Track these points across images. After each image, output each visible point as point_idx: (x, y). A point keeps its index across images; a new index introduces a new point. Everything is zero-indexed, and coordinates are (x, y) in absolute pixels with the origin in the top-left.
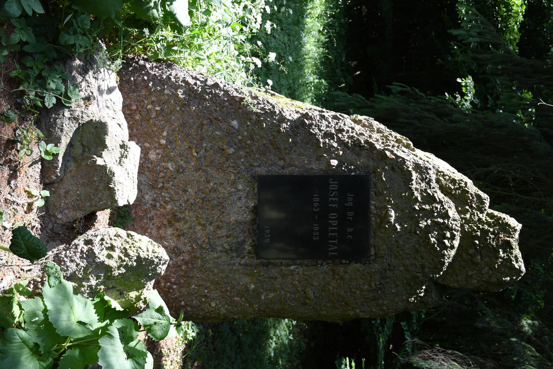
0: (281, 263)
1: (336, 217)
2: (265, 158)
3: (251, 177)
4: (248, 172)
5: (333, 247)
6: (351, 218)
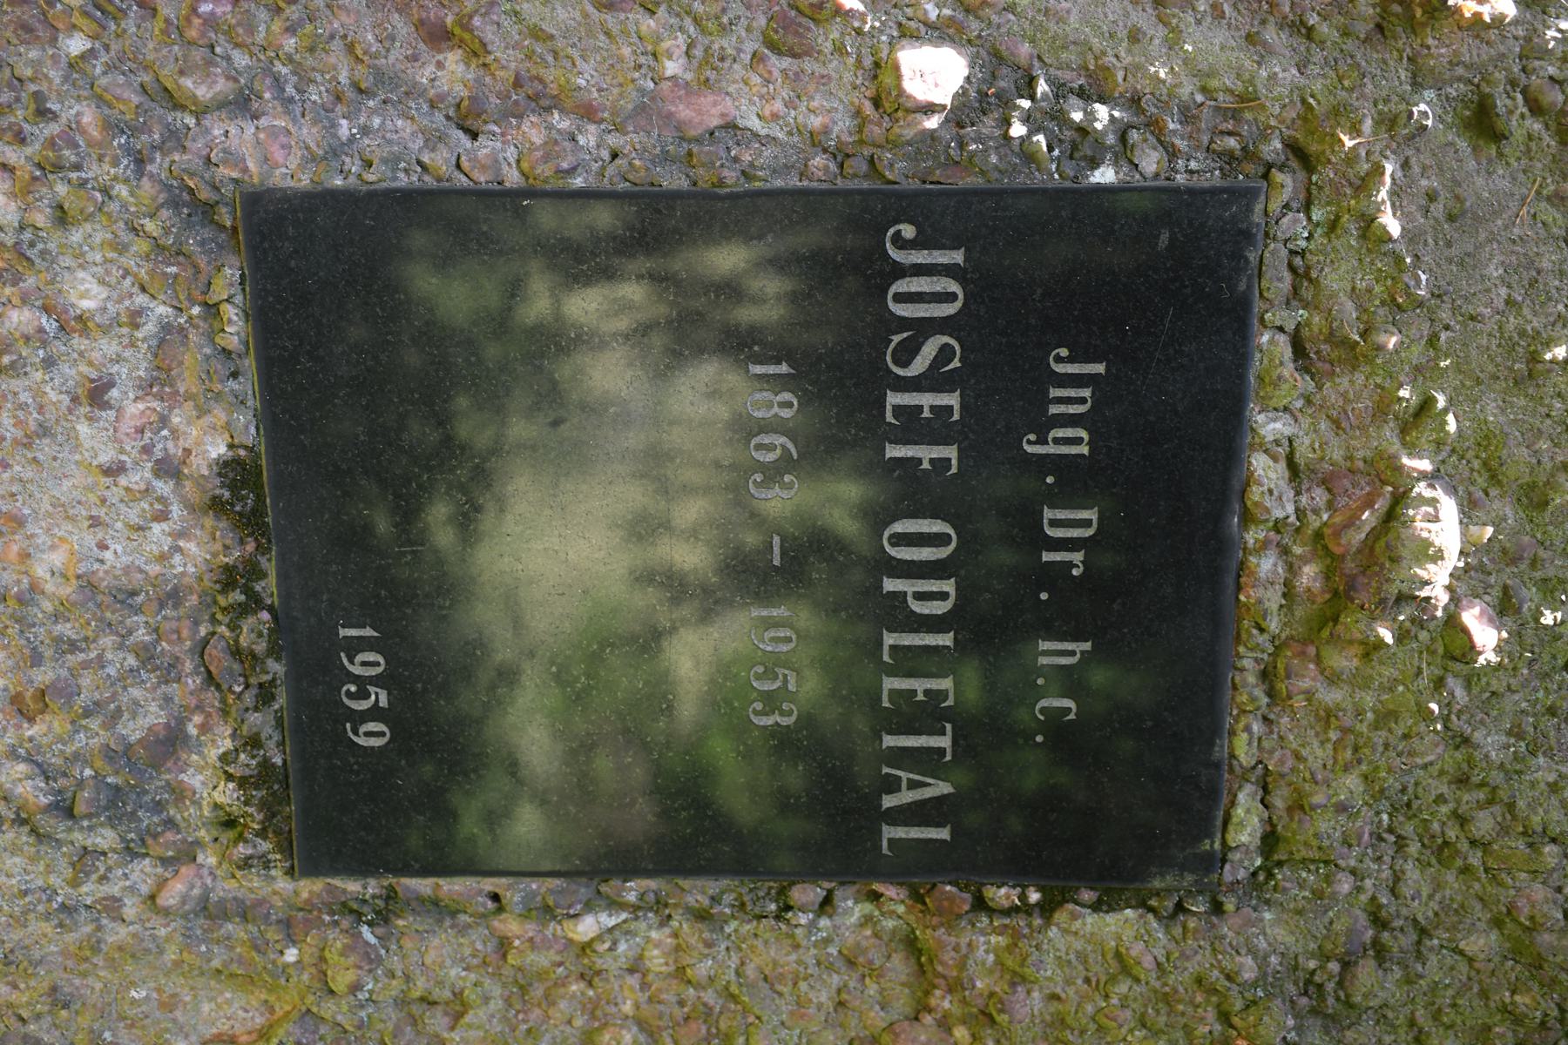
0: (495, 897)
1: (943, 553)
2: (291, 30)
3: (174, 204)
4: (140, 161)
5: (913, 785)
6: (1077, 557)
